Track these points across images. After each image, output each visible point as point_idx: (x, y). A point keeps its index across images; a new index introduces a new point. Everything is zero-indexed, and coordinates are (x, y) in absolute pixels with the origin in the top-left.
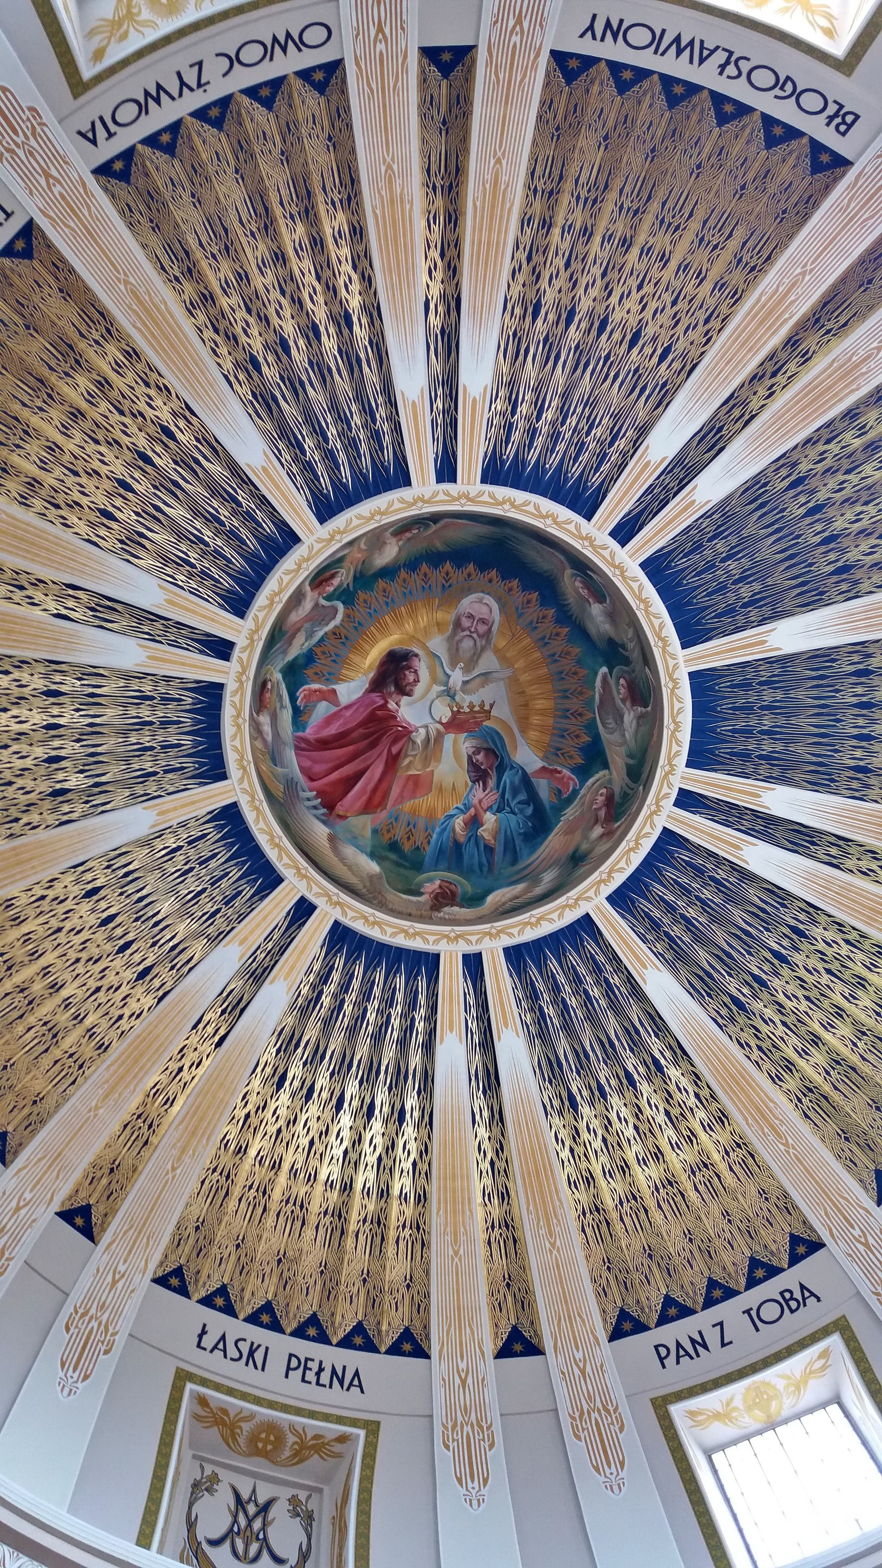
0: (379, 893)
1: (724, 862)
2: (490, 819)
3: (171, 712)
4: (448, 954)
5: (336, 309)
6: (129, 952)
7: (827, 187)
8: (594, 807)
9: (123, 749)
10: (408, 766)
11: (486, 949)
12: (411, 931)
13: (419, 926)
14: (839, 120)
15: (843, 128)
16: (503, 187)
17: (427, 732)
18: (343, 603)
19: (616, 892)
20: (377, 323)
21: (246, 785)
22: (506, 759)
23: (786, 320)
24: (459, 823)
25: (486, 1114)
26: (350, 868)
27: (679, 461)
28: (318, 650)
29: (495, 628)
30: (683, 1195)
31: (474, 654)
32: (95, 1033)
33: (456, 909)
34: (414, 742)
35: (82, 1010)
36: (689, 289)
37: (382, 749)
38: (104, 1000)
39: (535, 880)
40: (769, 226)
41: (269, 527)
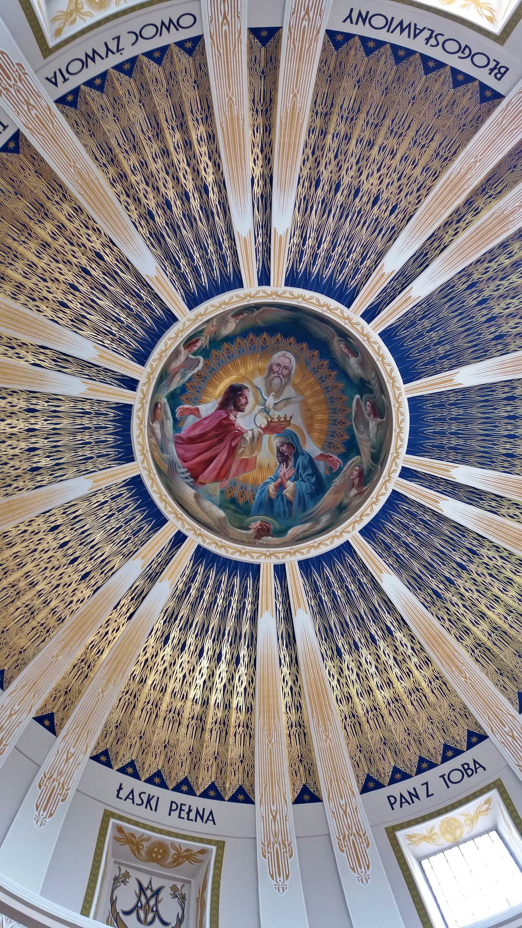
0: (225, 528)
1: (429, 510)
2: (290, 485)
3: (101, 421)
4: (265, 565)
5: (199, 183)
6: (76, 563)
7: (490, 111)
8: (352, 477)
9: (73, 443)
10: (242, 454)
11: (288, 562)
12: (243, 551)
13: (248, 548)
14: (496, 71)
15: (499, 76)
16: (298, 111)
17: (253, 434)
18: (203, 357)
19: (365, 528)
20: (223, 191)
21: (145, 465)
22: (299, 449)
23: (465, 190)
24: (271, 487)
25: (287, 659)
26: (207, 514)
27: (402, 273)
28: (188, 385)
29: (293, 372)
30: (404, 708)
31: (281, 387)
32: (56, 611)
33: (270, 538)
34: (245, 439)
35: (49, 598)
36: (408, 171)
37: (226, 444)
38: (61, 592)
39: (317, 521)
40: (455, 134)
41: (159, 312)
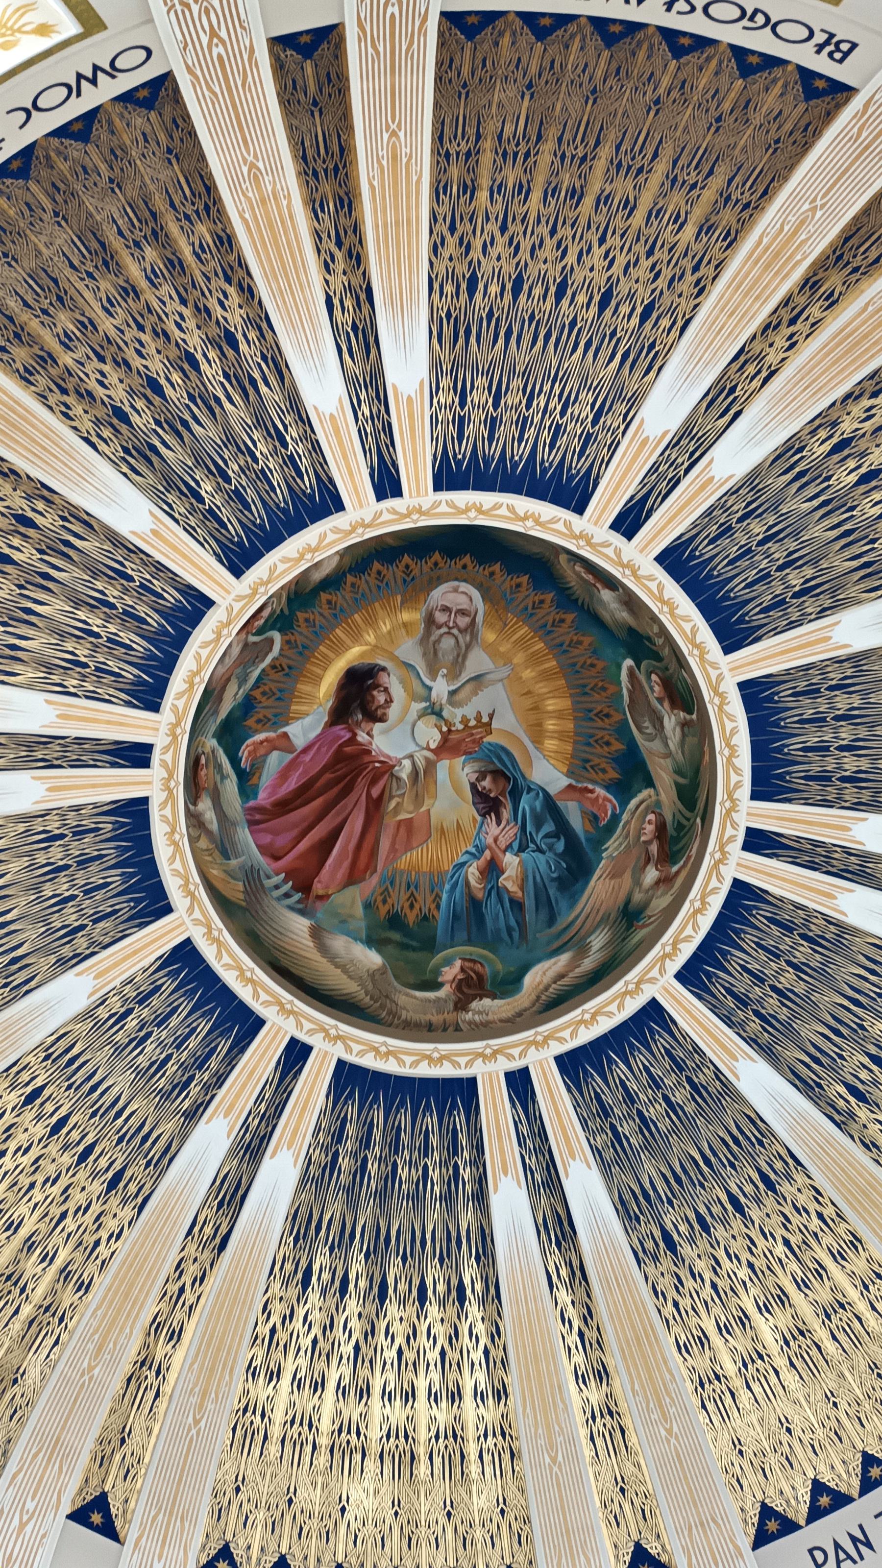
0: (387, 997)
1: (816, 914)
2: (511, 862)
3: (88, 845)
4: (486, 1077)
5: (214, 331)
6: (92, 1158)
7: (828, 114)
8: (643, 838)
9: (38, 908)
10: (397, 810)
11: (533, 1063)
12: (436, 1055)
13: (445, 1047)
14: (831, 48)
15: (838, 56)
16: (404, 160)
17: (414, 764)
18: (280, 631)
19: (685, 967)
20: (269, 335)
21: (197, 914)
22: (520, 780)
23: (799, 262)
24: (473, 872)
25: (564, 1272)
26: (345, 971)
27: (687, 431)
28: (257, 693)
29: (480, 619)
30: (819, 1348)
31: (458, 656)
32: (70, 1272)
33: (487, 1002)
34: (399, 779)
35: (50, 1247)
36: (667, 235)
37: (359, 794)
38: (72, 1227)
39: (583, 950)
40: (762, 160)
41: (172, 596)
